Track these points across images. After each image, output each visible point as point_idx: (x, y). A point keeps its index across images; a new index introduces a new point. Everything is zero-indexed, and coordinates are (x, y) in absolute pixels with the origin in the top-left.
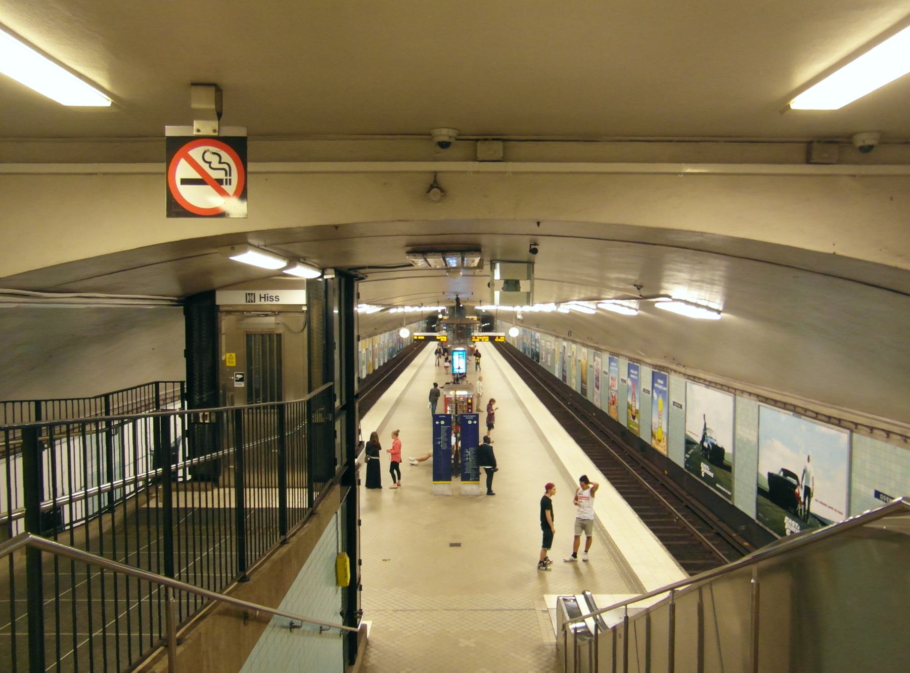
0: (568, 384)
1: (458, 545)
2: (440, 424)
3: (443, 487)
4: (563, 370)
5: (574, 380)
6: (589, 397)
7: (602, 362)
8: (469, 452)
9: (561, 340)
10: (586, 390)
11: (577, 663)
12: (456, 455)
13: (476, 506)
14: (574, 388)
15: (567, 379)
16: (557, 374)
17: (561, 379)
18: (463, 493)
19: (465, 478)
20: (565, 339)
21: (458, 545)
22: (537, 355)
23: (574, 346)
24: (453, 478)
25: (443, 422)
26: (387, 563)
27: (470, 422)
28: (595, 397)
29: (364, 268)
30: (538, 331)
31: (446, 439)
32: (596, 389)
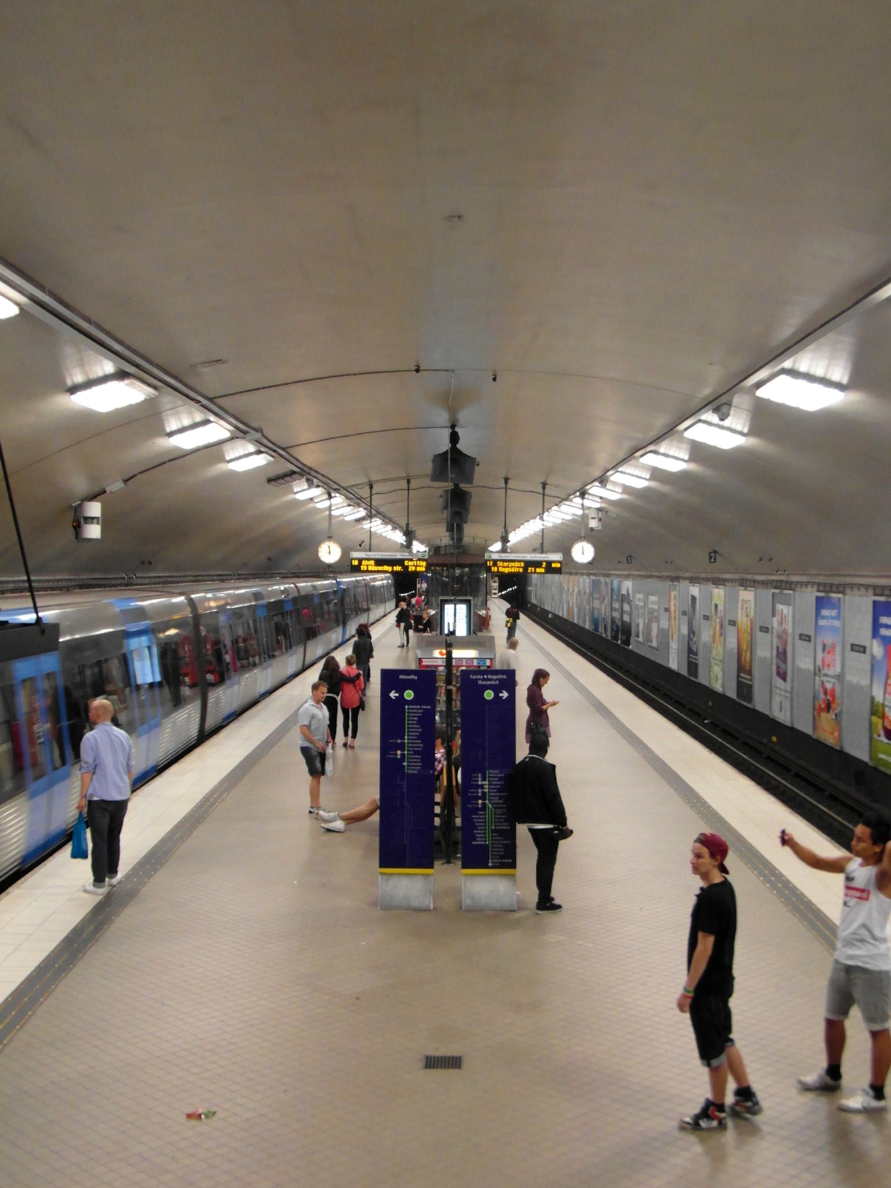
0: (702, 679)
1: (454, 1062)
2: (401, 699)
3: (409, 885)
4: (690, 651)
5: (717, 670)
6: (760, 703)
7: (792, 612)
8: (487, 784)
9: (684, 584)
10: (750, 688)
11: (6, 854)
12: (448, 803)
13: (508, 940)
14: (718, 687)
15: (701, 671)
16: (675, 662)
17: (684, 672)
18: (467, 902)
19: (476, 859)
20: (693, 580)
21: (454, 1062)
22: (625, 631)
23: (719, 593)
24: (437, 864)
25: (409, 695)
26: (204, 1127)
27: (489, 695)
28: (777, 699)
29: (301, 706)
30: (627, 577)
31: (419, 745)
32: (778, 682)
